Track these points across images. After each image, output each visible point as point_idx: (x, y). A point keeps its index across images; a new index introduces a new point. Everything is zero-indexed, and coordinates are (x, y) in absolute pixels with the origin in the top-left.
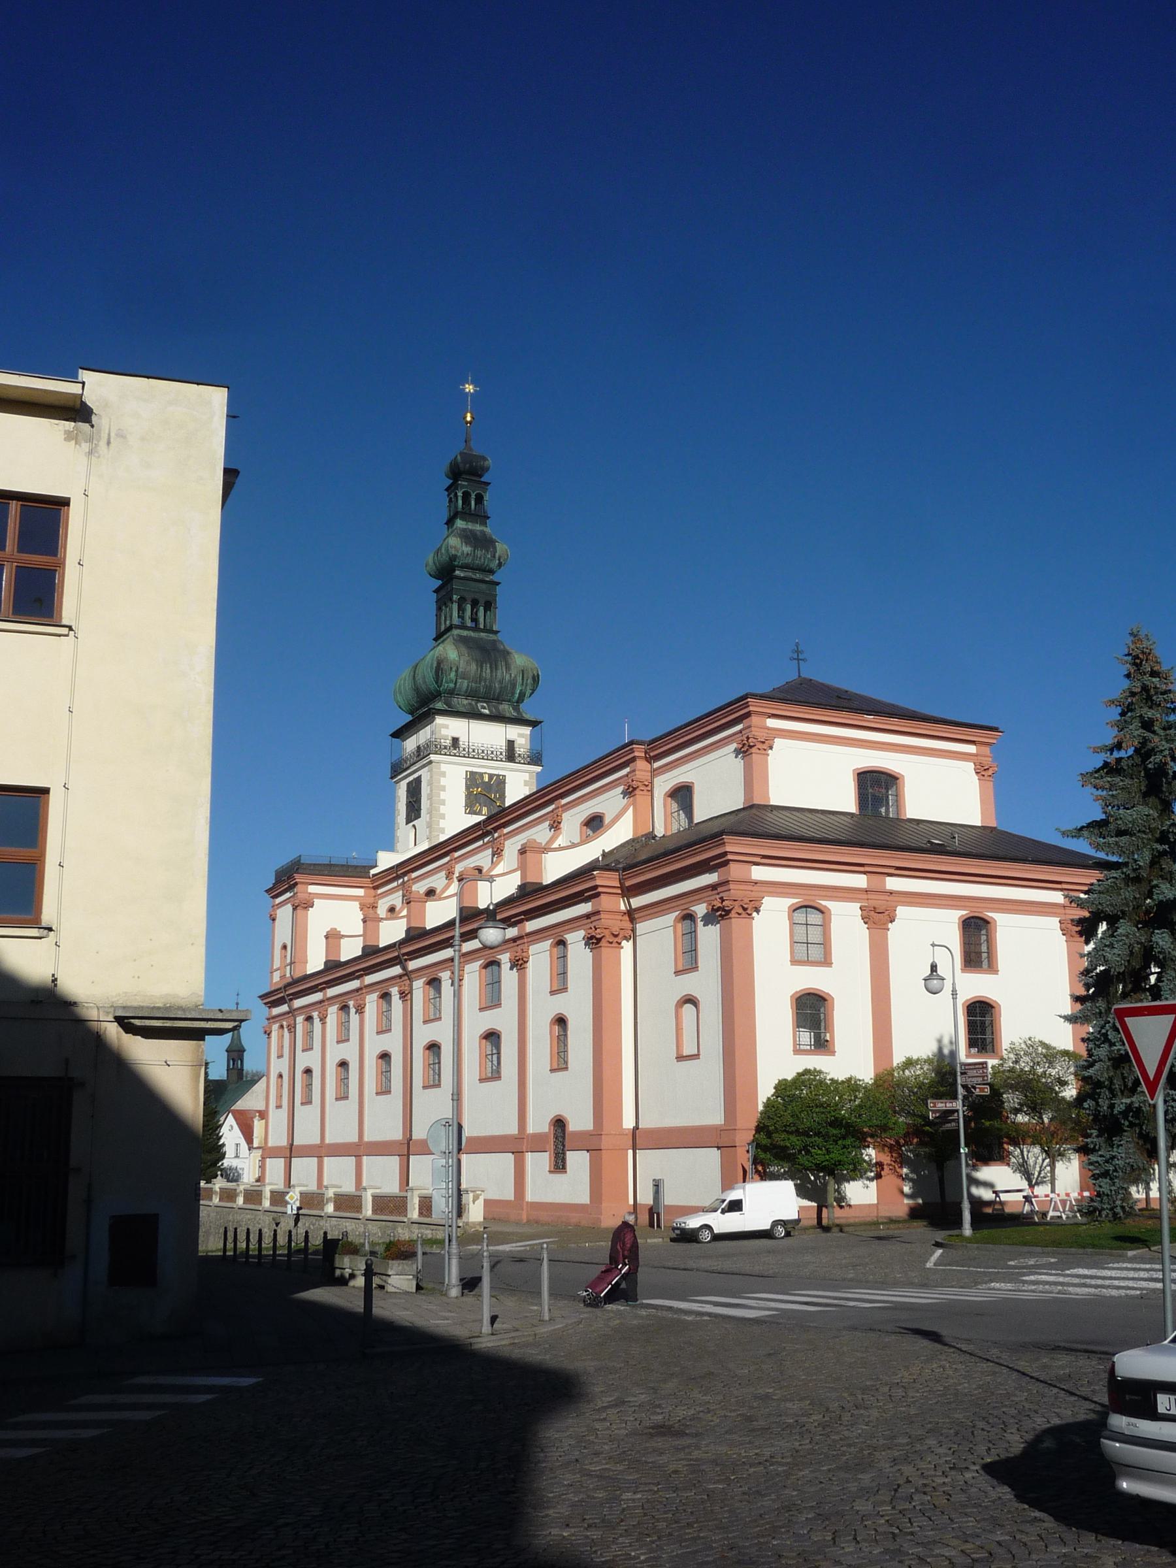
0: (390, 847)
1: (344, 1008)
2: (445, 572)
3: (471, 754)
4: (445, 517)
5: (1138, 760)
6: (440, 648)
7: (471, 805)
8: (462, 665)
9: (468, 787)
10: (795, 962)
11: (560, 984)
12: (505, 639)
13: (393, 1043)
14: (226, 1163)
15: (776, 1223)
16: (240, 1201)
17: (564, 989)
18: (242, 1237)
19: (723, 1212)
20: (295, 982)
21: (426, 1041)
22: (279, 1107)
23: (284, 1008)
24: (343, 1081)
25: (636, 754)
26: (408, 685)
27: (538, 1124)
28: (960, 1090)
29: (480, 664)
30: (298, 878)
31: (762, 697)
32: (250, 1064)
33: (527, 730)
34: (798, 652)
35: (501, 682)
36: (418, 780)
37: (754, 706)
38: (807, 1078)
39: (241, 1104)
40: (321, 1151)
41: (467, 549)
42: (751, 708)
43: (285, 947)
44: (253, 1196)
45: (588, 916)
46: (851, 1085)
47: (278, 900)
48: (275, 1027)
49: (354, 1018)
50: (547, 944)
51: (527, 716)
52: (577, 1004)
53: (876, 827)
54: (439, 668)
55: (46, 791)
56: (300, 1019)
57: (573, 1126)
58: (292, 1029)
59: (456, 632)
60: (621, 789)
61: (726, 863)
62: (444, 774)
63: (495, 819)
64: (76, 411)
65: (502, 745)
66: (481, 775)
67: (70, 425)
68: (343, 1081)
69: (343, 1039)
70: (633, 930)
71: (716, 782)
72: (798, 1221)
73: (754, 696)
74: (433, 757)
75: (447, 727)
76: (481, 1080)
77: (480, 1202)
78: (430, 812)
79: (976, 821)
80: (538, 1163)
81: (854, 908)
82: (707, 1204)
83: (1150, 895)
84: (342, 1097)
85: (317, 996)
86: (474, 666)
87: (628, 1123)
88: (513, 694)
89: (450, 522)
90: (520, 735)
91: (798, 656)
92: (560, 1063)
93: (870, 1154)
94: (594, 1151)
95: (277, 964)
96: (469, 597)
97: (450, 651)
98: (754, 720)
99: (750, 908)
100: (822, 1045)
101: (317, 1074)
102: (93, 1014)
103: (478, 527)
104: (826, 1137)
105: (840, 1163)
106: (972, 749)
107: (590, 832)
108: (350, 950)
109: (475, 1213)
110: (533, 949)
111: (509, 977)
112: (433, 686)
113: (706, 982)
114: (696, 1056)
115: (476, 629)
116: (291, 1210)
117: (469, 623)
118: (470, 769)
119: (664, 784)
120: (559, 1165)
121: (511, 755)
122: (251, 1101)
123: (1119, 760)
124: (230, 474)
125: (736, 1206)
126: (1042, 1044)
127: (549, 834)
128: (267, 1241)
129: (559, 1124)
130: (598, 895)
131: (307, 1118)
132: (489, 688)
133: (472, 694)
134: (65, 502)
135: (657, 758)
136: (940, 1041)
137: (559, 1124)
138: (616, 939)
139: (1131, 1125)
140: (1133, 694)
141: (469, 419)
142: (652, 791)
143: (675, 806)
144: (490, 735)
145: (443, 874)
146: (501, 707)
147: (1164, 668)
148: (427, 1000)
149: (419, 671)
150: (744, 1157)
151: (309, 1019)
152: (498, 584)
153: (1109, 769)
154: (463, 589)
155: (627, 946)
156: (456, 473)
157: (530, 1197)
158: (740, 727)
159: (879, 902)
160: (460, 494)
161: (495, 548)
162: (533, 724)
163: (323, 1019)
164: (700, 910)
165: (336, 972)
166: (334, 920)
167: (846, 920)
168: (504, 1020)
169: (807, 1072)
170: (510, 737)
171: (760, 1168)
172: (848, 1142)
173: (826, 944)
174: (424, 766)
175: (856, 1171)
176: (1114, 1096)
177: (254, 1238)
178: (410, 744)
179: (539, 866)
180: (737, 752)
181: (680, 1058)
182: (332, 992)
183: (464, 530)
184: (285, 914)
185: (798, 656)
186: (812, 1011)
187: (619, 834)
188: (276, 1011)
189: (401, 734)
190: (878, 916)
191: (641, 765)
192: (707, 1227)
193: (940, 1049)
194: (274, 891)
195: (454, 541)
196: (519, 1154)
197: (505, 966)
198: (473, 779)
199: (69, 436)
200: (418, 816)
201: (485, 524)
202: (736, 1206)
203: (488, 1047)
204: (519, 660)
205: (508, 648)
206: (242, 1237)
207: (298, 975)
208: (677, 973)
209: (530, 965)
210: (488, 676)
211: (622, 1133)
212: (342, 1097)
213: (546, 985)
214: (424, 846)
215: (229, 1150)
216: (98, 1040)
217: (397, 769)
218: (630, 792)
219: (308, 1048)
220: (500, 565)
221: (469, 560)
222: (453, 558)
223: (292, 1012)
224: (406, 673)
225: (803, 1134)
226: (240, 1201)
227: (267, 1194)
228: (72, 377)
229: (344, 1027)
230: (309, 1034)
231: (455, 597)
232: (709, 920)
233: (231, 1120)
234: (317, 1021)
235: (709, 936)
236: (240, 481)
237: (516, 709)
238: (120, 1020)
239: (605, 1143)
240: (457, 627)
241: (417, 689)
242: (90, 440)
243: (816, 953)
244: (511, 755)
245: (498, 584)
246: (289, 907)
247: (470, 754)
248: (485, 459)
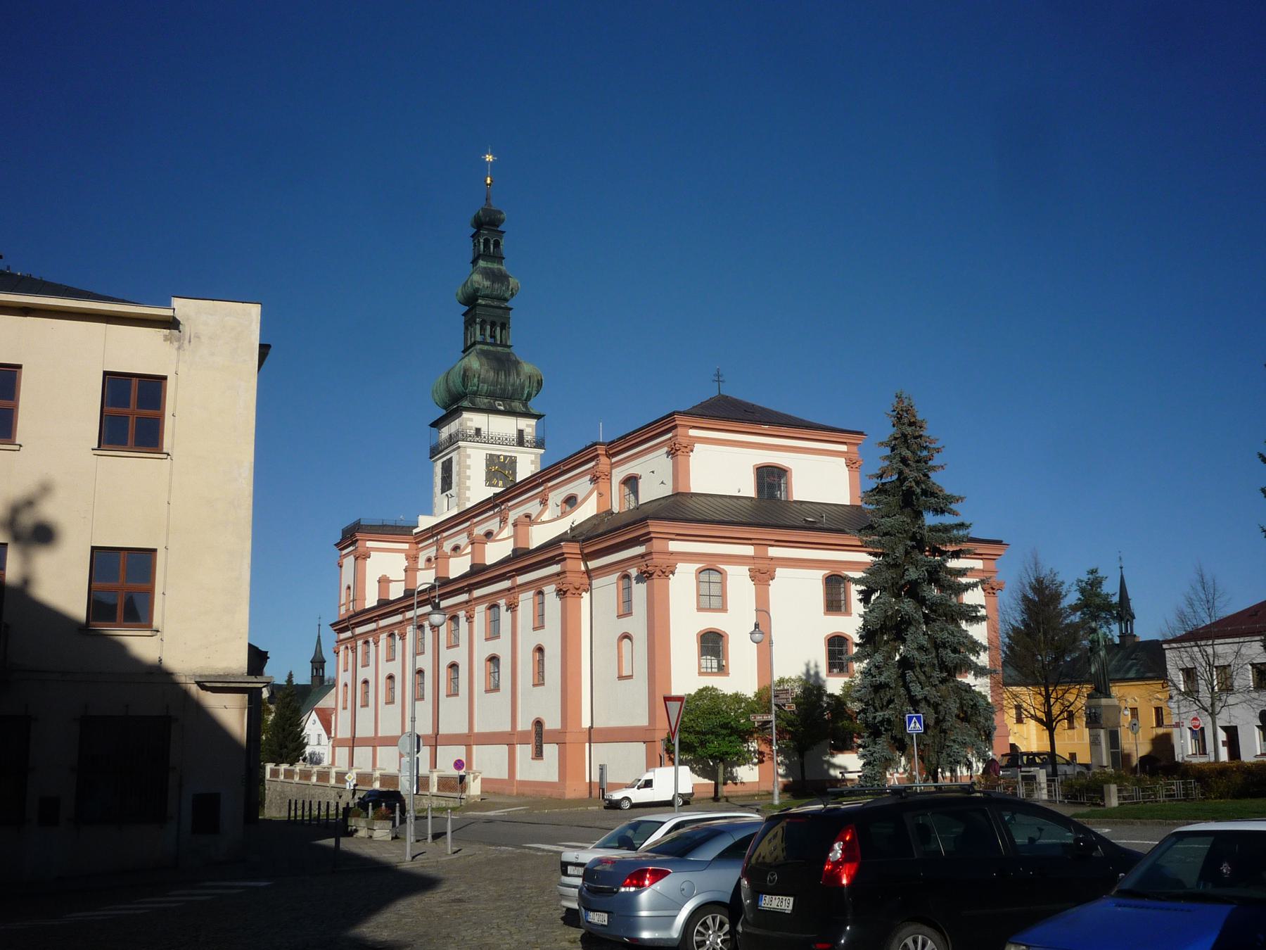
0: (429, 512)
1: (392, 635)
2: (471, 300)
3: (490, 440)
4: (471, 259)
5: (898, 483)
6: (466, 359)
7: (490, 479)
8: (483, 373)
9: (487, 466)
10: (700, 609)
11: (539, 625)
12: (517, 352)
13: (425, 662)
14: (308, 750)
16: (314, 779)
17: (542, 627)
18: (315, 807)
19: (639, 788)
20: (357, 614)
21: (448, 662)
22: (345, 708)
23: (348, 634)
24: (391, 690)
26: (443, 387)
27: (525, 724)
28: (774, 708)
29: (497, 373)
30: (359, 536)
31: (685, 413)
32: (328, 673)
33: (533, 422)
37: (679, 420)
38: (703, 693)
39: (322, 704)
40: (376, 742)
41: (487, 283)
43: (349, 588)
44: (323, 776)
45: (558, 574)
46: (737, 698)
47: (344, 552)
48: (342, 648)
49: (398, 643)
50: (531, 593)
51: (533, 411)
52: (551, 638)
53: (772, 511)
54: (465, 376)
55: (155, 550)
56: (360, 643)
57: (548, 726)
58: (354, 650)
59: (478, 347)
60: (588, 477)
61: (651, 539)
62: (469, 456)
63: (510, 492)
64: (171, 324)
65: (514, 433)
66: (499, 456)
67: (167, 332)
68: (391, 690)
69: (391, 659)
70: (590, 585)
71: (653, 474)
72: (692, 794)
73: (679, 413)
74: (460, 443)
75: (471, 420)
76: (487, 691)
77: (479, 781)
78: (458, 485)
79: (845, 499)
80: (524, 752)
81: (744, 571)
82: (629, 782)
83: (902, 577)
84: (390, 701)
85: (372, 626)
86: (492, 374)
87: (586, 723)
89: (474, 262)
91: (718, 378)
92: (539, 679)
93: (754, 746)
94: (561, 744)
95: (343, 601)
97: (473, 362)
98: (680, 430)
100: (722, 670)
101: (372, 684)
102: (182, 679)
103: (495, 266)
104: (717, 735)
105: (727, 753)
106: (844, 448)
107: (568, 509)
108: (396, 592)
109: (475, 789)
110: (522, 597)
111: (505, 616)
112: (461, 389)
113: (637, 624)
114: (630, 677)
115: (494, 344)
116: (349, 786)
117: (489, 340)
119: (619, 474)
120: (539, 754)
121: (521, 441)
122: (326, 702)
123: (883, 484)
124: (264, 349)
125: (648, 784)
127: (540, 508)
128: (332, 811)
129: (538, 723)
130: (565, 559)
131: (365, 716)
132: (504, 390)
133: (491, 395)
134: (165, 378)
135: (615, 455)
136: (807, 665)
137: (538, 723)
138: (578, 591)
139: (886, 730)
140: (896, 439)
142: (610, 479)
143: (627, 491)
144: (505, 426)
145: (465, 535)
147: (919, 418)
148: (449, 632)
149: (451, 378)
150: (660, 748)
151: (366, 642)
153: (880, 490)
154: (485, 314)
155: (586, 596)
156: (479, 224)
157: (518, 777)
158: (670, 435)
159: (762, 565)
162: (538, 417)
163: (376, 643)
164: (634, 572)
165: (385, 607)
166: (386, 568)
167: (739, 580)
168: (501, 647)
169: (706, 689)
170: (520, 427)
172: (732, 738)
173: (723, 596)
175: (743, 759)
176: (877, 711)
177: (323, 808)
178: (445, 432)
179: (527, 536)
180: (668, 453)
181: (621, 677)
182: (383, 623)
184: (349, 562)
185: (718, 378)
186: (712, 643)
187: (587, 510)
188: (343, 636)
189: (438, 424)
190: (762, 575)
191: (603, 460)
192: (627, 798)
193: (808, 671)
194: (341, 545)
195: (477, 278)
196: (511, 745)
197: (503, 608)
198: (491, 460)
199: (166, 339)
202: (648, 784)
203: (491, 666)
204: (527, 368)
206: (315, 807)
207: (358, 609)
208: (619, 616)
209: (519, 608)
211: (581, 731)
212: (390, 701)
213: (529, 623)
214: (454, 512)
215: (312, 740)
216: (186, 694)
217: (435, 451)
218: (594, 480)
219: (365, 665)
220: (512, 295)
221: (488, 292)
222: (477, 290)
223: (354, 637)
224: (441, 378)
225: (704, 733)
226: (314, 779)
227: (333, 774)
228: (167, 305)
229: (391, 648)
230: (366, 654)
232: (640, 579)
233: (314, 716)
234: (372, 644)
235: (639, 591)
236: (271, 352)
237: (525, 405)
238: (198, 683)
239: (569, 738)
240: (480, 343)
241: (449, 391)
242: (179, 340)
243: (716, 602)
244: (521, 441)
246: (352, 558)
247: (490, 440)
248: (500, 213)
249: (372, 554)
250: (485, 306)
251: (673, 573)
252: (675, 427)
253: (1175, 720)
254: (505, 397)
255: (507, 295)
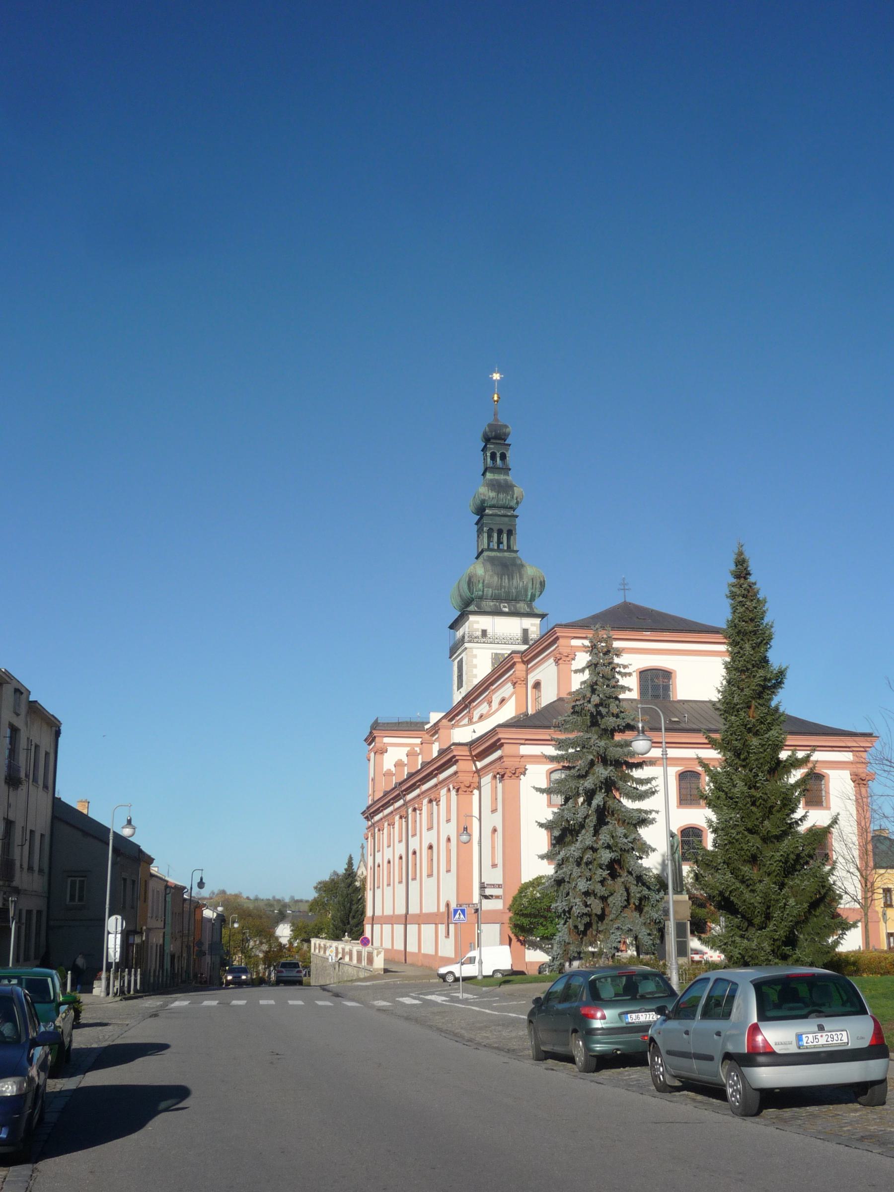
15: (495, 972)
25: (515, 660)
29: (501, 576)
31: (567, 626)
33: (537, 621)
34: (624, 584)
35: (516, 588)
36: (462, 659)
37: (560, 632)
41: (492, 494)
42: (558, 634)
51: (537, 611)
62: (475, 656)
65: (518, 633)
70: (479, 783)
75: (478, 622)
77: (382, 956)
86: (496, 579)
88: (527, 595)
89: (484, 474)
90: (532, 625)
91: (624, 587)
96: (495, 528)
99: (518, 773)
103: (502, 477)
112: (468, 594)
115: (499, 549)
118: (495, 651)
126: (320, 883)
132: (508, 593)
133: (496, 598)
141: (496, 398)
146: (518, 605)
152: (517, 517)
154: (495, 524)
156: (487, 439)
160: (489, 454)
161: (513, 492)
162: (542, 616)
170: (525, 627)
171: (521, 938)
174: (463, 651)
183: (491, 480)
185: (624, 587)
189: (455, 626)
192: (451, 973)
200: (462, 686)
201: (508, 475)
204: (530, 571)
205: (524, 562)
210: (507, 585)
220: (517, 503)
221: (494, 502)
222: (483, 501)
231: (485, 529)
245: (517, 517)
249: (389, 749)
250: (491, 515)
251: (524, 774)
252: (557, 639)
253: (817, 914)
254: (508, 599)
255: (513, 503)
